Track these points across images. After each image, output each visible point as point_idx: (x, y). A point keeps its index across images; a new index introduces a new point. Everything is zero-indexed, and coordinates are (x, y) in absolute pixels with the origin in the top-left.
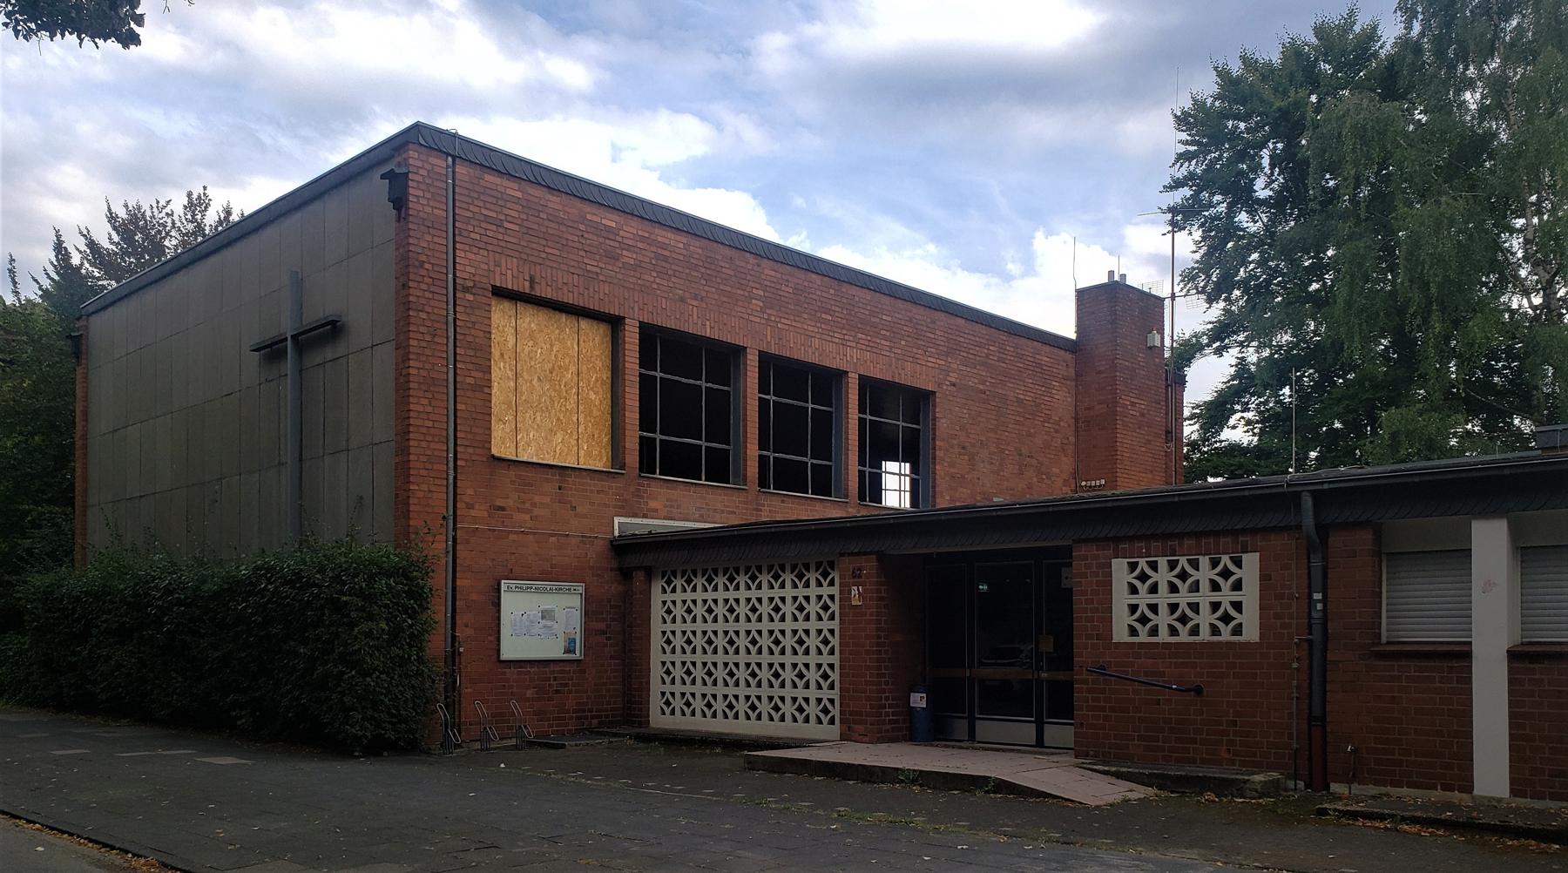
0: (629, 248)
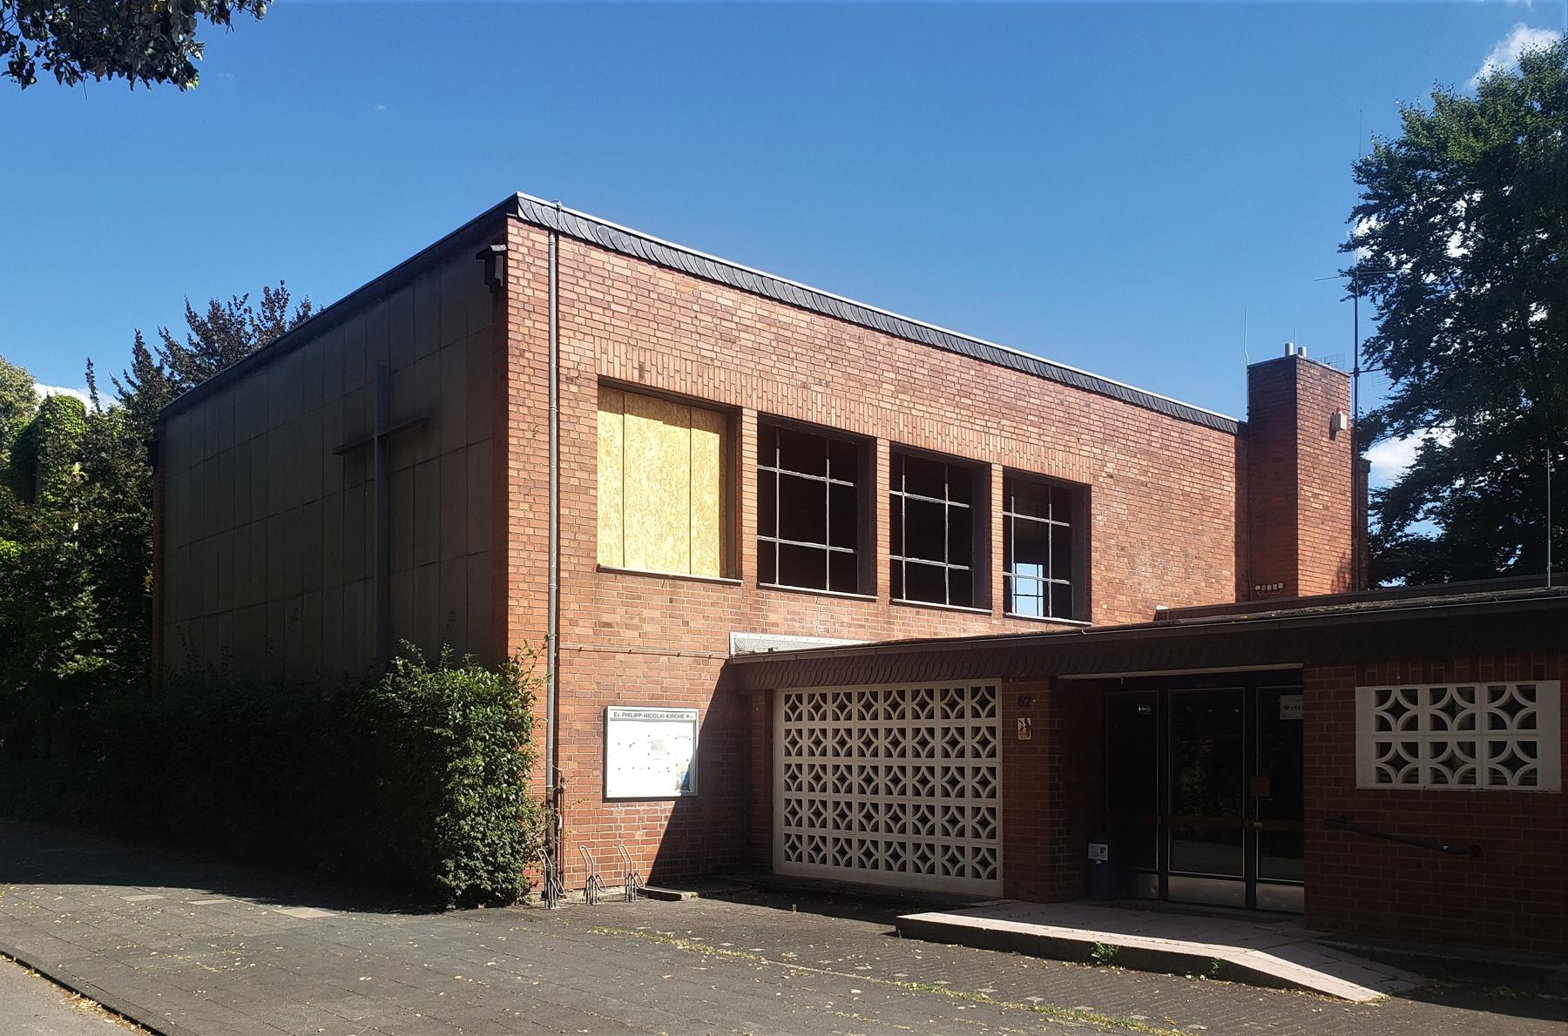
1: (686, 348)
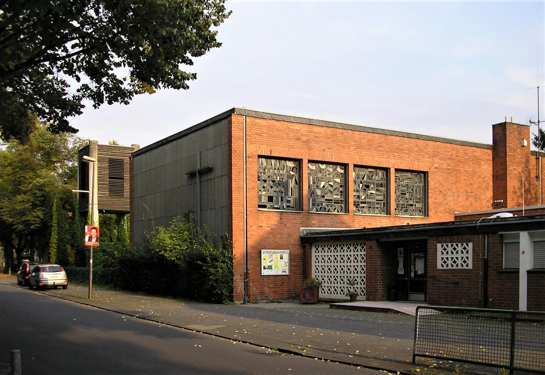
0: (304, 135)
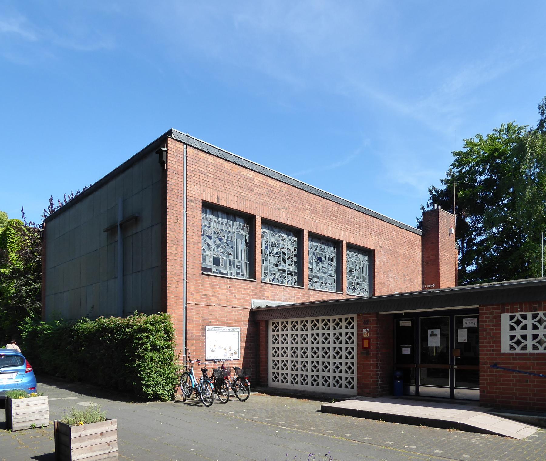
0: (258, 186)
1: (235, 192)
